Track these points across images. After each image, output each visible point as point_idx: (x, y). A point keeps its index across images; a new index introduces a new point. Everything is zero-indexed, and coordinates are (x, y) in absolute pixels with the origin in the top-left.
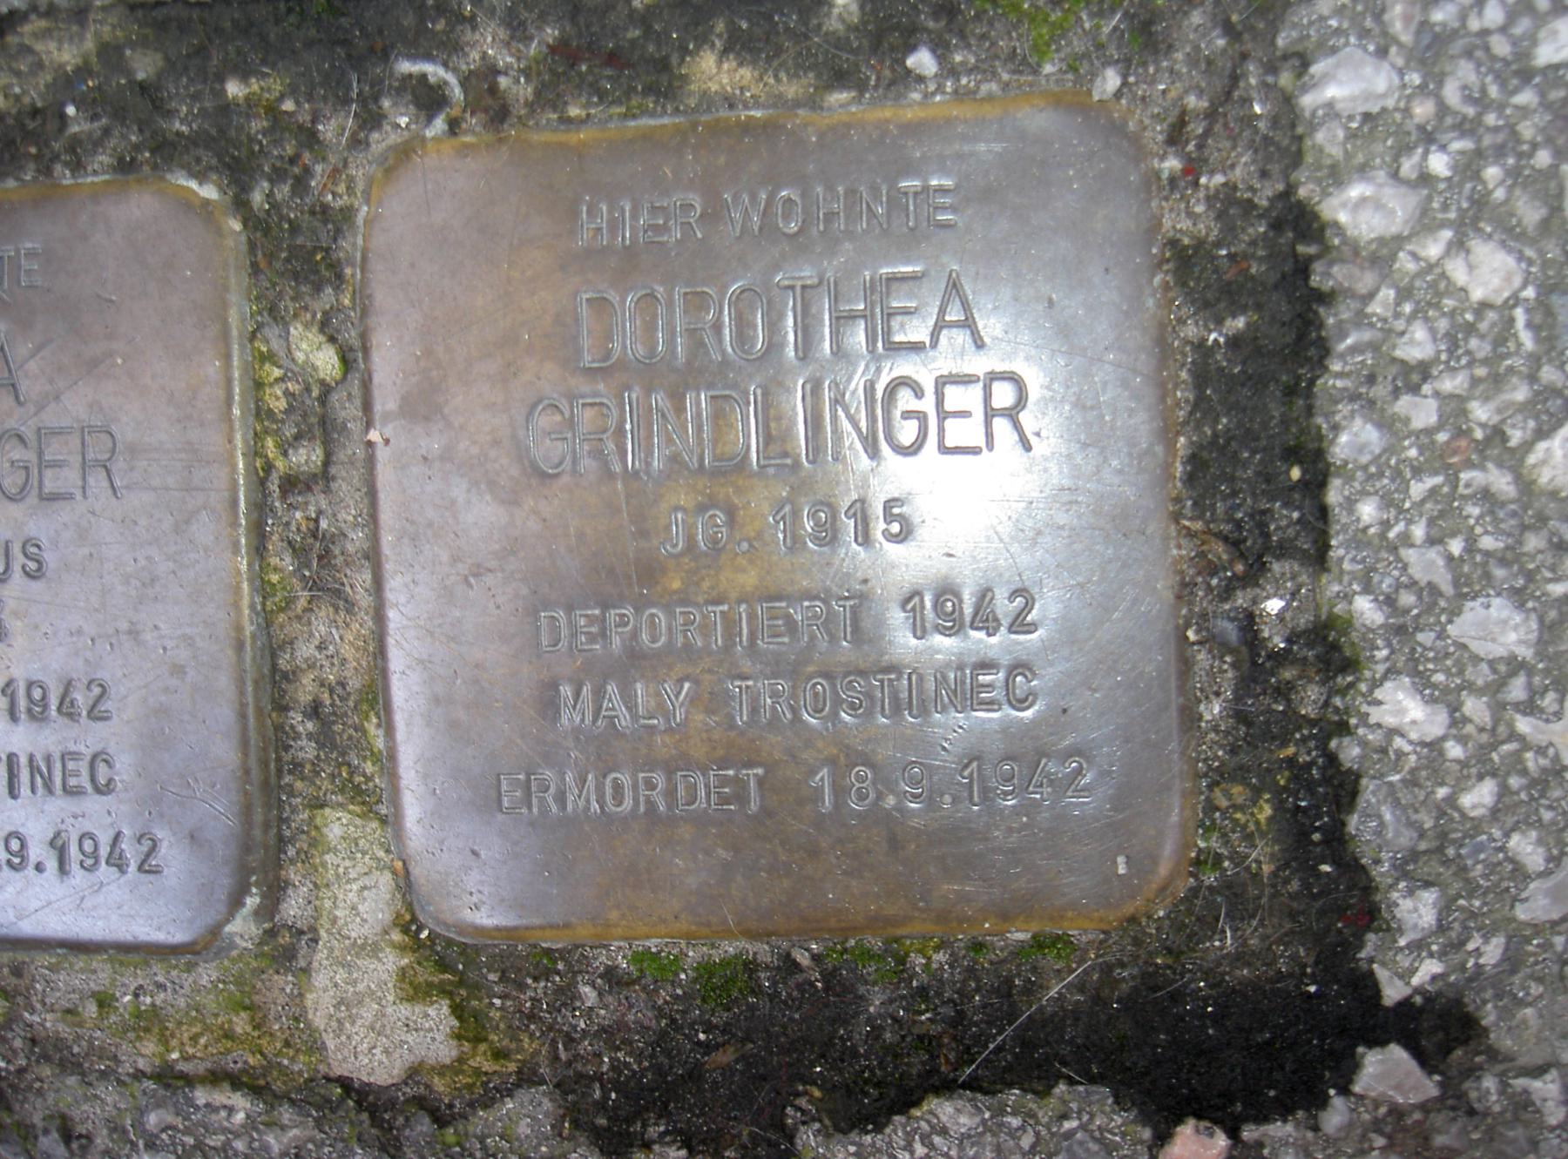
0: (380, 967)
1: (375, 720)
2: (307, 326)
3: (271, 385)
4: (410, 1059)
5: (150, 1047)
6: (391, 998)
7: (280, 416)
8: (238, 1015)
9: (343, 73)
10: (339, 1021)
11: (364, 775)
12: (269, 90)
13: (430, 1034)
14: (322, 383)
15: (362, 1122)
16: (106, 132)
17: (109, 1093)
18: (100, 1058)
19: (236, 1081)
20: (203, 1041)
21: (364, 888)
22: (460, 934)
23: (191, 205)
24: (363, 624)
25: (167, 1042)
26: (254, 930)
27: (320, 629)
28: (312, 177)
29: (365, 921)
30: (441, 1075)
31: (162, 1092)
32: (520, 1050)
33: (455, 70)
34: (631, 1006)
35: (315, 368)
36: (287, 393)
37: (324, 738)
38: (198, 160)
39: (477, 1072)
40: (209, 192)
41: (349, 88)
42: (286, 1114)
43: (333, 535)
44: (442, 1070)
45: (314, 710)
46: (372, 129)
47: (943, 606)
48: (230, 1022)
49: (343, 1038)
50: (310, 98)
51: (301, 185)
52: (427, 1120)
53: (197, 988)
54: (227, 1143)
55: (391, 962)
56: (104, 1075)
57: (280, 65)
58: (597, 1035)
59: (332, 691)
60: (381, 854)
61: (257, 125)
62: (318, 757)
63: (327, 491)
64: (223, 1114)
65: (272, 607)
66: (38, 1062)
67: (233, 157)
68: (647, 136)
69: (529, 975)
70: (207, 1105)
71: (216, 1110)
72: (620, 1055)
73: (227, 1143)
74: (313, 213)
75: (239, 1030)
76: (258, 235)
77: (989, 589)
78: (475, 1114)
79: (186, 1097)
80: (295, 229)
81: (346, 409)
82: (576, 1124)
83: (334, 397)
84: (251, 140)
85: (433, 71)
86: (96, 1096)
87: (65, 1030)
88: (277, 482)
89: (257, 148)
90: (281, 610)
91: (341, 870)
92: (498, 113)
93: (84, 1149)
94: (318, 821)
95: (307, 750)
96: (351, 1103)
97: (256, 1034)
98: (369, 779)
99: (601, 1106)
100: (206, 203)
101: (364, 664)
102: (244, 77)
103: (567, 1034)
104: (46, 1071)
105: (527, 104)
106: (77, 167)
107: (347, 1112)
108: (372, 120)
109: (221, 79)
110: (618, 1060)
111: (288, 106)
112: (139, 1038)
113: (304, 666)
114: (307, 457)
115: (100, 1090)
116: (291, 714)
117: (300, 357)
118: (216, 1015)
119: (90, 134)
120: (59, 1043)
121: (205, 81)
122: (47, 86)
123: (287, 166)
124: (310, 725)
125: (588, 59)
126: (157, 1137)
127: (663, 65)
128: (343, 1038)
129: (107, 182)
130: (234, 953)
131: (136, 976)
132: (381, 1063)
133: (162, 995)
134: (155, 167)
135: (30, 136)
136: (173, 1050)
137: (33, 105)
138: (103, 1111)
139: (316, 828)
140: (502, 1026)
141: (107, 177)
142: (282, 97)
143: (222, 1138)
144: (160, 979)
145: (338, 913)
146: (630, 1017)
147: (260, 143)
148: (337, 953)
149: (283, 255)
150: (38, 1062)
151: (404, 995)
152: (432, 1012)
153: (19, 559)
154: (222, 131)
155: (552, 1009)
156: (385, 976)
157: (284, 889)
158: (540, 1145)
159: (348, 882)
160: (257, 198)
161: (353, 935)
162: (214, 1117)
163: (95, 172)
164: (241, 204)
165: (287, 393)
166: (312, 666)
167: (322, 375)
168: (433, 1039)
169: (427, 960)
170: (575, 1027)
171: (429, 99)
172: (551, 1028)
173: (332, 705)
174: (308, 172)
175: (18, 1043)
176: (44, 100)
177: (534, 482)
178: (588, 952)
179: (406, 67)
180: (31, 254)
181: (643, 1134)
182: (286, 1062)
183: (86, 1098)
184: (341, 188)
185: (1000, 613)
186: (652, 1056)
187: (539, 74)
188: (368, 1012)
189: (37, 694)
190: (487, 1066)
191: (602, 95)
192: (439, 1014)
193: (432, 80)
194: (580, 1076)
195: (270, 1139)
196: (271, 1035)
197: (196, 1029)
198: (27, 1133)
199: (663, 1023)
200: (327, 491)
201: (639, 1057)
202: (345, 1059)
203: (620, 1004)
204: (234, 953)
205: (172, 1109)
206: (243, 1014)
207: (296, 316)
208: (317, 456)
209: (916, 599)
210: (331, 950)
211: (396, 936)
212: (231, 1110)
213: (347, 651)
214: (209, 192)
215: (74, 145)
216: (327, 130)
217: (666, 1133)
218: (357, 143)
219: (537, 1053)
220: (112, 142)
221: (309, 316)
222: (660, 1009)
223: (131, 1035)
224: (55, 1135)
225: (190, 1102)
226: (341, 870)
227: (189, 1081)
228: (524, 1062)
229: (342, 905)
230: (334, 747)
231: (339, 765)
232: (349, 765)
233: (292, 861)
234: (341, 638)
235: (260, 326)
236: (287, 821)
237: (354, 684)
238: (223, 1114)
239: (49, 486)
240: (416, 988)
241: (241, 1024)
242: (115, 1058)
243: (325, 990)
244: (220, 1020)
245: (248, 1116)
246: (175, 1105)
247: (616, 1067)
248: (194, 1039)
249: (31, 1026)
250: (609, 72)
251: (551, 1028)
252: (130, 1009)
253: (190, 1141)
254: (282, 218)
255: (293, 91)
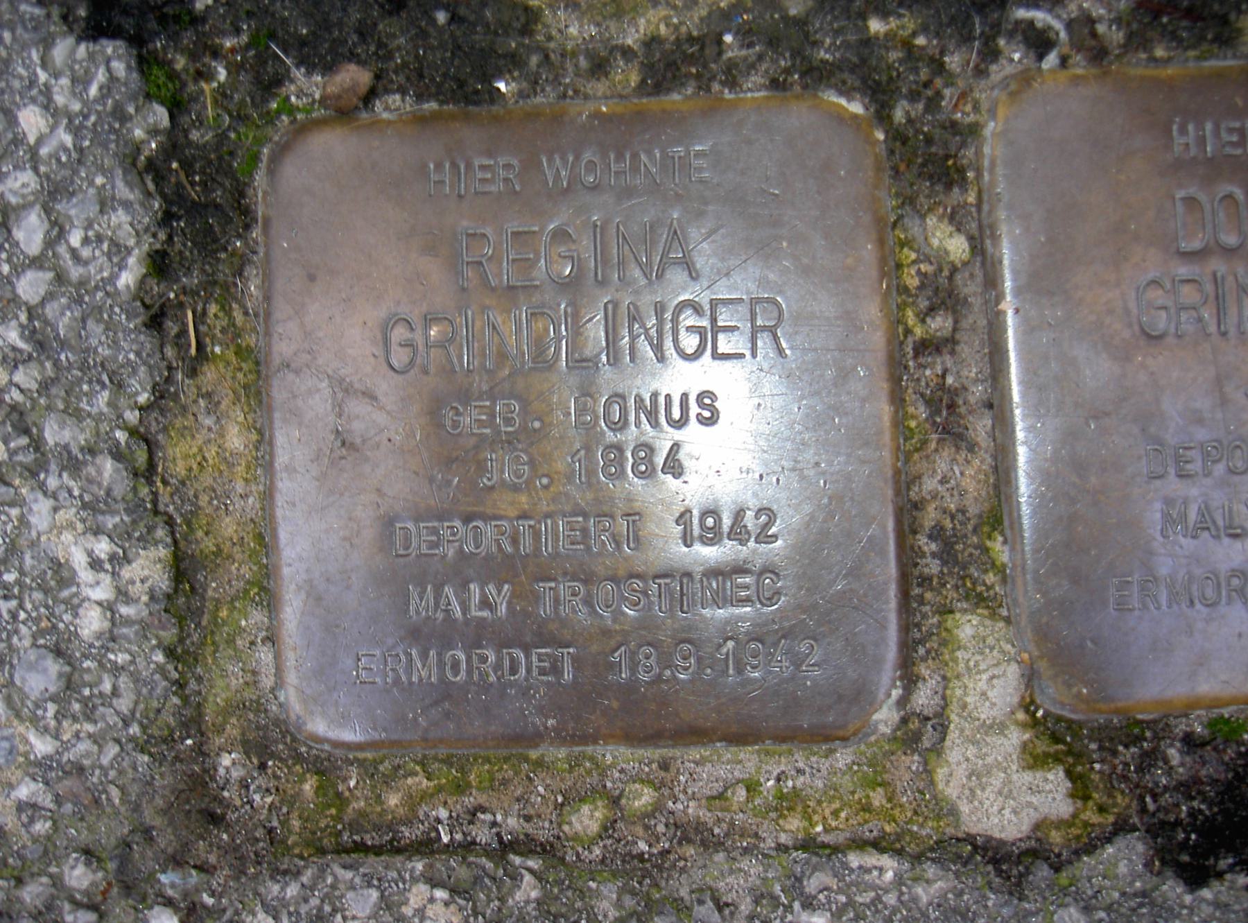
0: (1006, 742)
1: (1000, 539)
2: (941, 219)
3: (909, 266)
4: (1035, 816)
5: (794, 823)
6: (1014, 768)
7: (914, 292)
8: (874, 790)
9: (969, 17)
10: (971, 789)
11: (985, 585)
12: (903, 27)
13: (1051, 795)
14: (952, 263)
15: (989, 873)
16: (760, 57)
17: (752, 866)
18: (742, 836)
19: (877, 845)
20: (843, 815)
21: (992, 678)
22: (1072, 711)
23: (842, 118)
24: (981, 462)
25: (810, 819)
26: (896, 717)
27: (942, 466)
28: (942, 98)
29: (995, 704)
30: (1058, 828)
31: (815, 859)
32: (1115, 805)
33: (1058, 17)
34: (1204, 764)
35: (947, 252)
36: (919, 272)
37: (947, 554)
38: (844, 82)
39: (1086, 824)
40: (856, 108)
41: (972, 30)
42: (931, 870)
43: (956, 389)
44: (1060, 824)
45: (937, 533)
46: (992, 62)
47: (706, 524)
48: (868, 797)
49: (976, 803)
50: (937, 35)
51: (933, 104)
52: (1046, 867)
53: (833, 772)
54: (878, 898)
55: (1016, 737)
56: (746, 851)
57: (914, 7)
58: (1176, 789)
59: (953, 517)
60: (1008, 647)
61: (894, 55)
62: (941, 572)
63: (953, 353)
64: (875, 873)
65: (908, 450)
66: (680, 843)
67: (875, 81)
68: (1219, 74)
69: (1121, 743)
70: (860, 867)
71: (868, 871)
72: (1195, 804)
73: (878, 898)
74: (944, 128)
75: (876, 803)
76: (898, 144)
77: (743, 510)
78: (1079, 859)
79: (842, 863)
80: (929, 140)
81: (970, 288)
82: (1164, 862)
83: (958, 277)
84: (890, 67)
85: (1040, 17)
86: (740, 870)
87: (706, 816)
88: (911, 346)
89: (895, 74)
90: (917, 450)
91: (972, 664)
92: (1099, 54)
93: (732, 914)
94: (949, 624)
95: (933, 567)
96: (979, 858)
97: (889, 806)
98: (989, 588)
99: (1184, 846)
100: (855, 117)
101: (984, 493)
102: (885, 15)
103: (1152, 790)
104: (690, 851)
105: (1120, 46)
106: (732, 84)
107: (976, 865)
108: (991, 54)
109: (863, 16)
110: (1193, 808)
111: (921, 41)
112: (782, 816)
113: (929, 497)
114: (940, 324)
115: (744, 864)
116: (918, 536)
117: (935, 242)
118: (853, 793)
119: (745, 59)
120: (699, 827)
121: (849, 18)
122: (702, 19)
123: (921, 89)
124: (933, 547)
125: (1169, 14)
126: (815, 897)
127: (1224, 21)
128: (976, 803)
129: (767, 98)
130: (873, 738)
131: (779, 763)
132: (1010, 821)
133: (802, 779)
134: (805, 87)
135: (690, 59)
136: (817, 823)
137: (689, 34)
138: (746, 881)
139: (946, 629)
140: (1101, 786)
141: (762, 94)
142: (914, 34)
143: (873, 894)
144: (801, 765)
145: (968, 699)
146: (1203, 772)
147: (897, 70)
148: (967, 732)
149: (920, 160)
150: (680, 843)
151: (1024, 764)
152: (1050, 776)
153: (694, 409)
154: (864, 61)
155: (1140, 769)
156: (1010, 750)
157: (915, 683)
158: (1134, 881)
159: (979, 672)
160: (899, 115)
161: (983, 716)
162: (867, 877)
163: (750, 90)
164: (882, 115)
165: (919, 272)
166: (934, 497)
167: (952, 258)
168: (1054, 799)
169: (1043, 734)
170: (1156, 784)
171: (1039, 42)
172: (1137, 786)
173: (954, 529)
174: (939, 95)
175: (661, 828)
176: (700, 30)
177: (1142, 343)
178: (1172, 721)
179: (1022, 13)
180: (698, 155)
181: (1215, 866)
182: (915, 828)
183: (732, 871)
184: (968, 108)
185: (750, 526)
186: (1222, 802)
187: (1128, 24)
188: (997, 780)
189: (710, 522)
190: (1095, 819)
191: (1180, 41)
192: (1055, 780)
193: (1039, 25)
194: (1163, 823)
195: (919, 890)
196: (901, 806)
197: (837, 805)
198: (680, 907)
199: (1230, 775)
200: (953, 353)
201: (1211, 805)
202: (979, 820)
203: (1195, 762)
204: (873, 738)
205: (830, 873)
206: (879, 790)
207: (930, 210)
208: (949, 323)
209: (688, 515)
210: (962, 731)
211: (1021, 716)
212: (881, 870)
213: (970, 485)
214: (856, 108)
215: (731, 66)
216: (953, 61)
217: (1235, 865)
218: (980, 72)
219: (1128, 807)
220: (764, 66)
221: (941, 210)
222: (1227, 764)
223: (773, 815)
224: (710, 904)
225: (845, 865)
226: (972, 664)
227: (836, 849)
228: (1119, 814)
229: (972, 692)
230: (956, 563)
231: (963, 578)
232: (970, 577)
233: (924, 659)
234: (962, 474)
235: (900, 217)
236: (918, 625)
237: (973, 510)
238: (875, 873)
239: (723, 348)
240: (1035, 758)
241: (878, 798)
242: (756, 835)
243: (959, 764)
244: (856, 797)
245: (895, 875)
246: (832, 869)
247: (1193, 813)
248: (835, 814)
249: (673, 813)
250: (1184, 23)
251: (1137, 786)
252: (773, 792)
253: (843, 899)
254: (918, 132)
255: (924, 29)
